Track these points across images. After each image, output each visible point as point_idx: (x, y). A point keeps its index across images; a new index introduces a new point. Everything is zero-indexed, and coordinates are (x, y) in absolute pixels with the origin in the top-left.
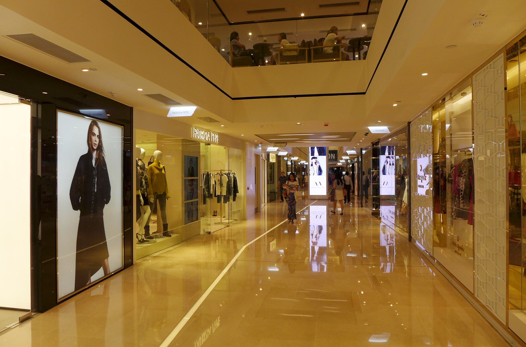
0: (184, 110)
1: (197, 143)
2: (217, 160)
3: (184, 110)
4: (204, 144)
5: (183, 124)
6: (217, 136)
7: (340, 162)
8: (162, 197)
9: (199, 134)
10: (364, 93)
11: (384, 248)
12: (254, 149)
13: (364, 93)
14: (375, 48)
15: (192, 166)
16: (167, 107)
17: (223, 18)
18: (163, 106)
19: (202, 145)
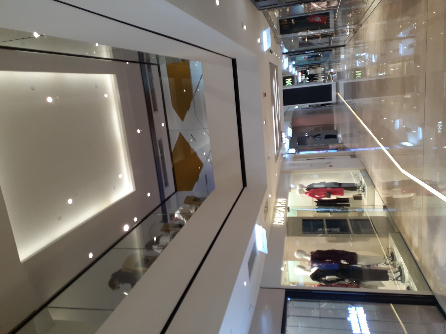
0: (260, 238)
1: (289, 220)
2: (299, 202)
3: (260, 238)
4: (288, 213)
5: (274, 235)
6: (279, 200)
7: (295, 74)
8: (339, 188)
9: (279, 219)
10: (234, 61)
11: (329, 197)
12: (288, 162)
13: (234, 61)
14: (178, 52)
15: (309, 226)
16: (258, 254)
17: (35, 319)
18: (258, 260)
19: (290, 215)
